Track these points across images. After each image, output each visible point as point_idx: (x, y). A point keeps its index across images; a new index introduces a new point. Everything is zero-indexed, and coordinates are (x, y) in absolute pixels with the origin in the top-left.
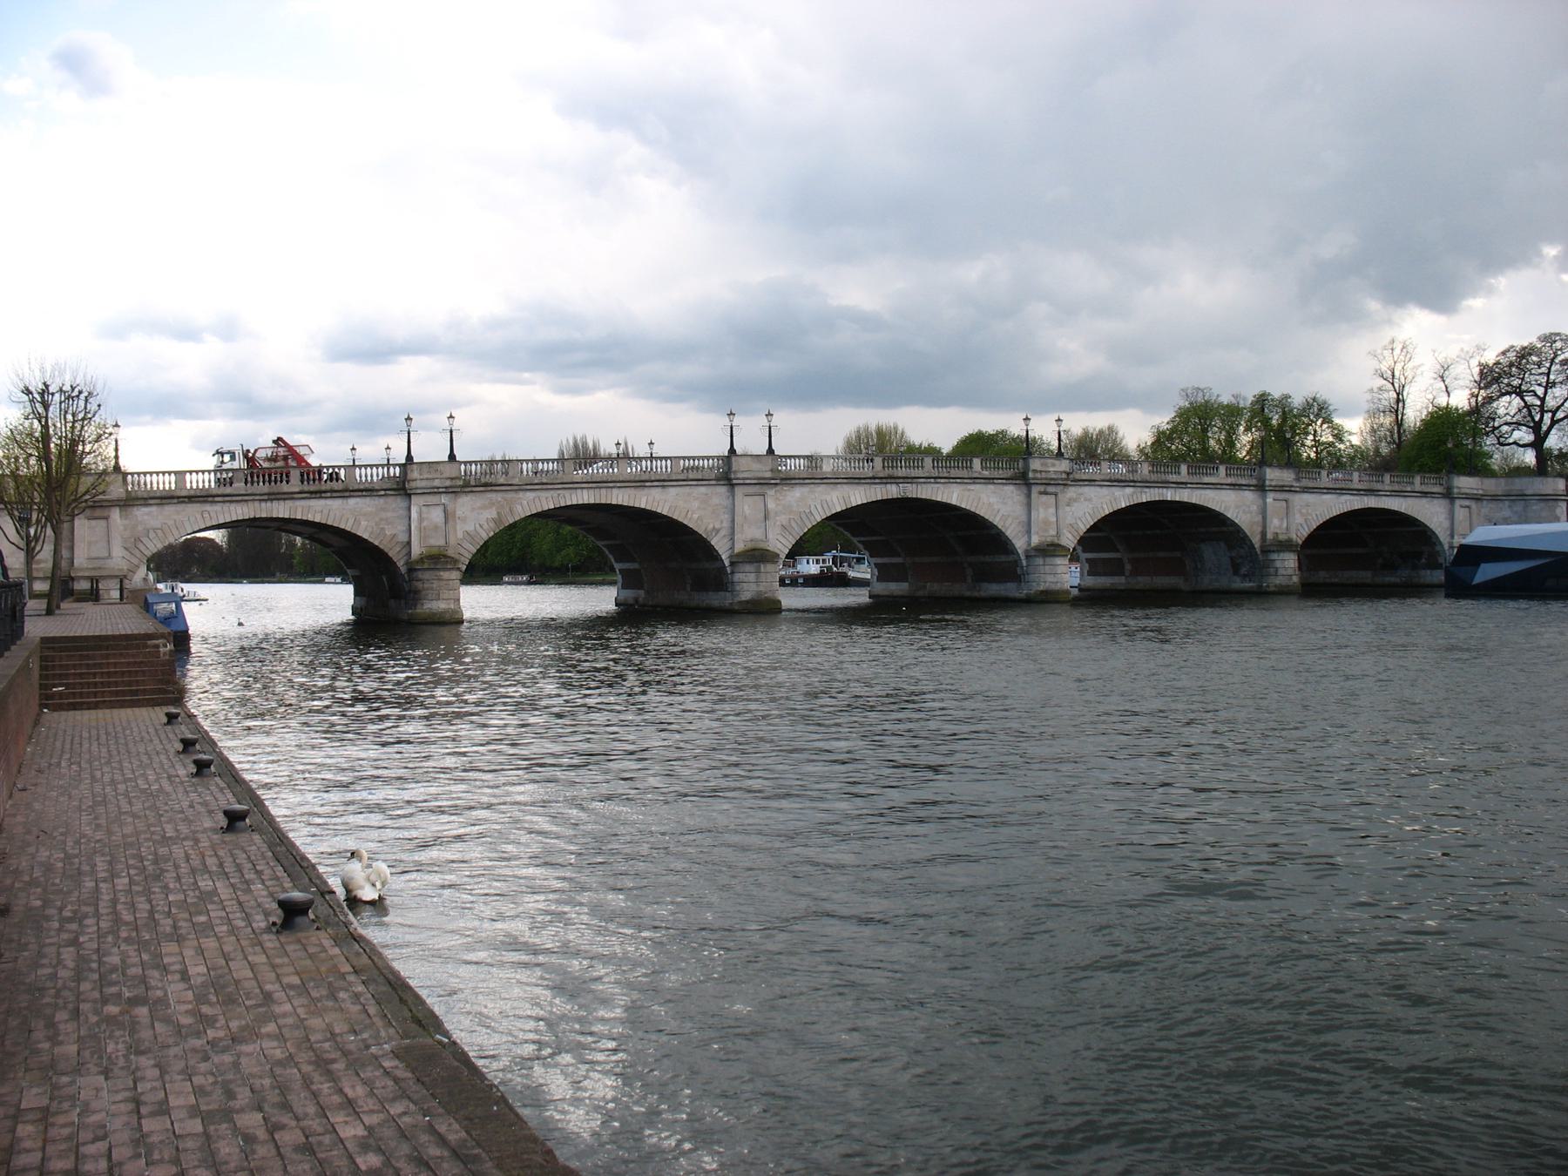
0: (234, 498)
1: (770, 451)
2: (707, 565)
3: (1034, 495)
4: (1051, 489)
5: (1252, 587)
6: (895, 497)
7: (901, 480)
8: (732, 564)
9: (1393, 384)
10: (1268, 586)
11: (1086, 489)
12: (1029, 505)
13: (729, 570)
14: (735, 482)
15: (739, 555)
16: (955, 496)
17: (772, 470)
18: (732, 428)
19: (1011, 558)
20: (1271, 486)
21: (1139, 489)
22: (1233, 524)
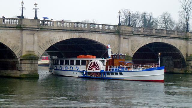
0: (30, 29)
1: (36, 18)
2: (8, 60)
3: (122, 39)
4: (127, 37)
5: (183, 72)
6: (78, 37)
7: (80, 32)
8: (21, 60)
9: (186, 10)
10: (188, 72)
11: (137, 37)
12: (119, 42)
13: (20, 62)
14: (24, 29)
15: (24, 57)
16: (97, 37)
17: (37, 25)
18: (36, 9)
19: (14, 60)
20: (190, 39)
21: (152, 38)
22: (6, 47)
